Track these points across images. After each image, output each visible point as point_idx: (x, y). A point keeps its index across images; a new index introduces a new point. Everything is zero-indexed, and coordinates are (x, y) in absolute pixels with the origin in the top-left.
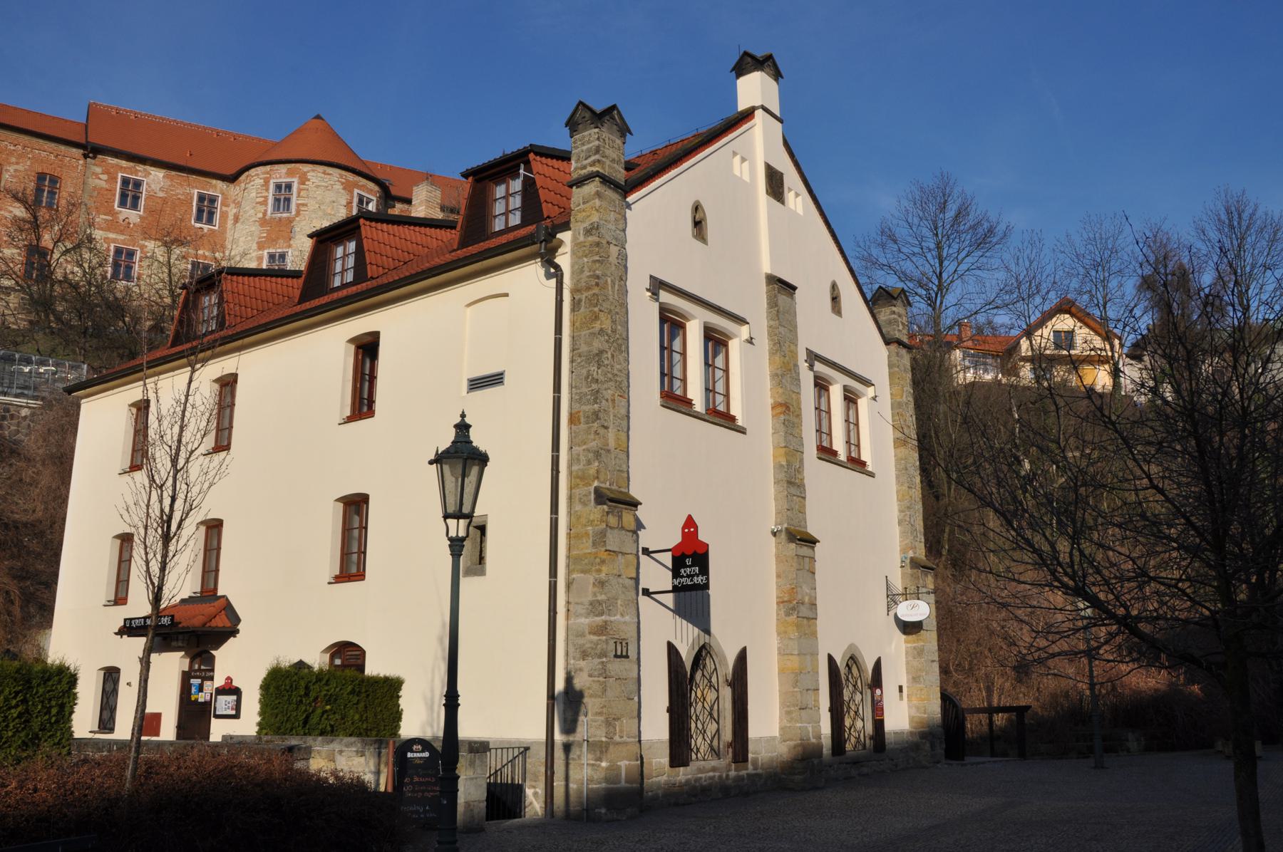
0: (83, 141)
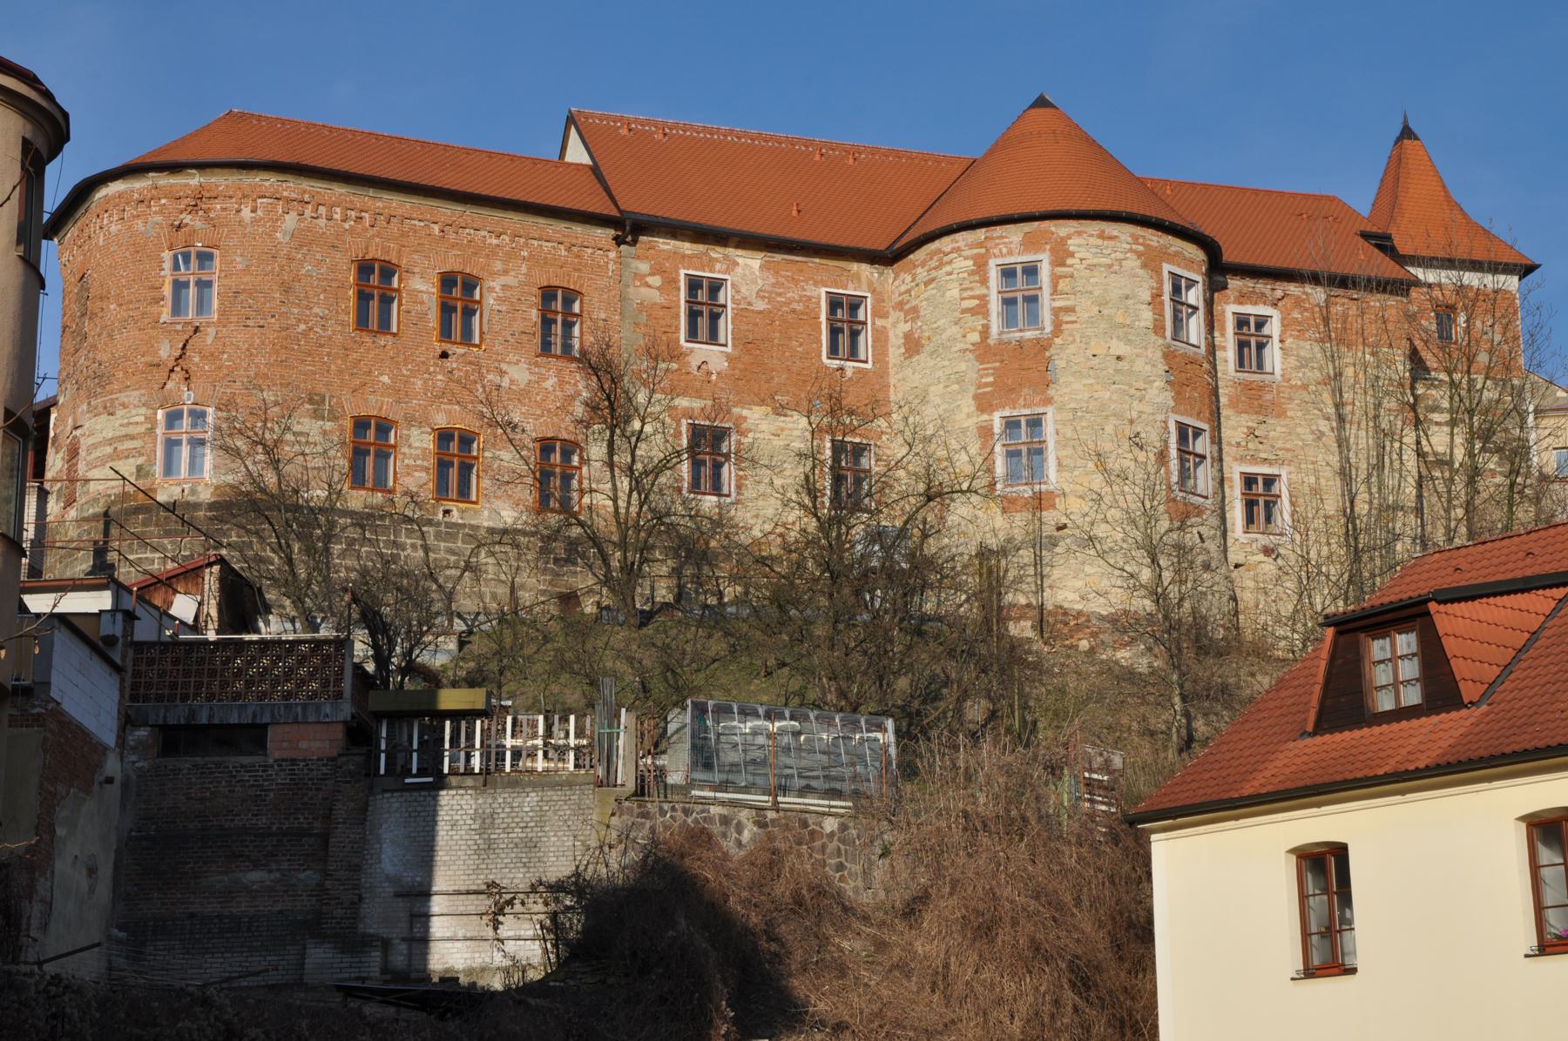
0: (614, 213)
